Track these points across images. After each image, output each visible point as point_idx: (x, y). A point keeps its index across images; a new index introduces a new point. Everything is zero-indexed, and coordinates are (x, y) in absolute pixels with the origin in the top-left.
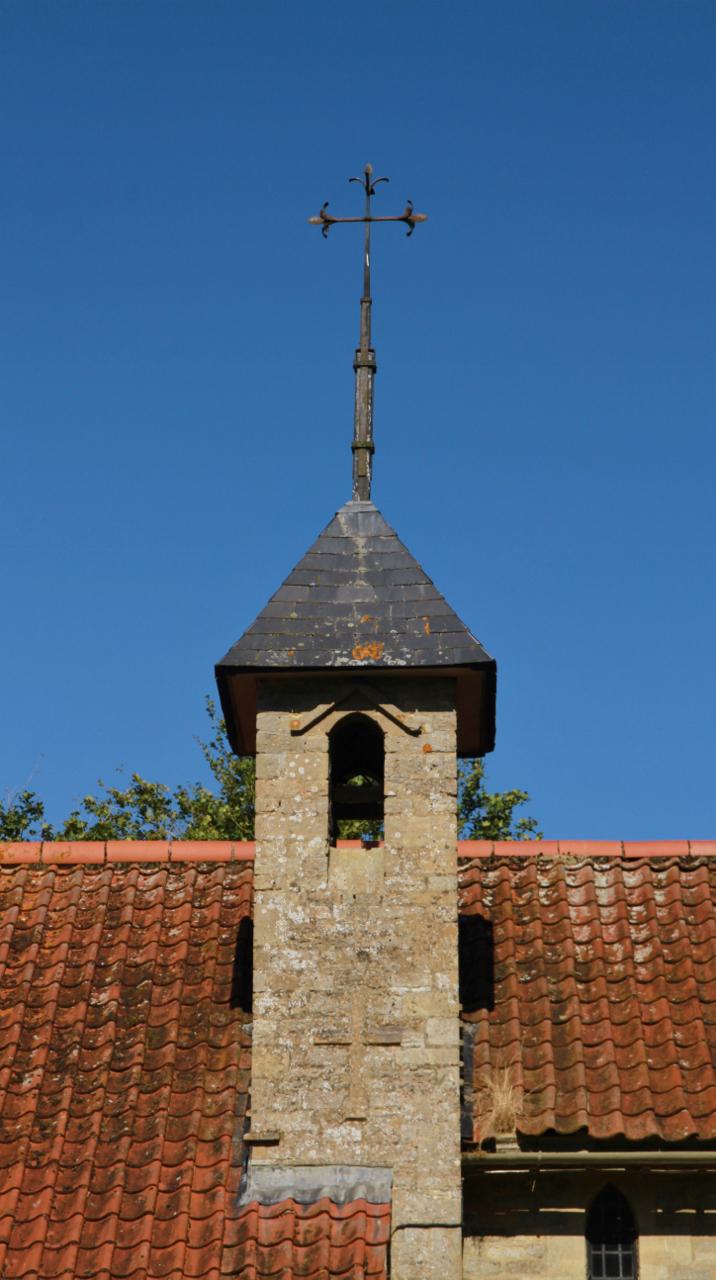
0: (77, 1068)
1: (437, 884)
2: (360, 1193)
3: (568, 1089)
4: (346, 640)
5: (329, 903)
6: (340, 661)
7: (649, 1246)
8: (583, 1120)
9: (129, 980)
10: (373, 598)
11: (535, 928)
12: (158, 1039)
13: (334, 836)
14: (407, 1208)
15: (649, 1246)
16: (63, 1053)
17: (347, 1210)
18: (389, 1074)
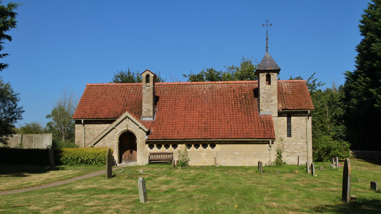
0: (242, 103)
1: (276, 88)
2: (269, 114)
3: (285, 105)
4: (267, 67)
5: (266, 90)
6: (267, 69)
7: (292, 118)
8: (287, 108)
9: (245, 95)
10: (269, 63)
11: (280, 89)
12: (249, 100)
13: (266, 85)
14: (273, 115)
15: (292, 118)
16: (241, 102)
17: (269, 116)
18: (272, 105)
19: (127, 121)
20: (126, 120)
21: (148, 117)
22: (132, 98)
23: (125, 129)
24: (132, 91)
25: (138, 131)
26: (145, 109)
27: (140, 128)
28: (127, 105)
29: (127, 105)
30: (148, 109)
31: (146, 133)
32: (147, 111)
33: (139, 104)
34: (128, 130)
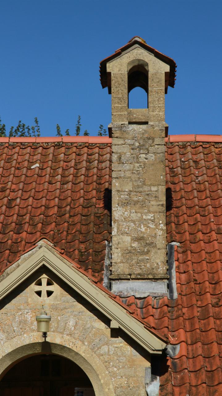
19: (44, 293)
20: (38, 288)
21: (141, 278)
22: (41, 195)
23: (36, 338)
24: (37, 165)
25: (105, 349)
26: (128, 239)
27: (117, 333)
28: (20, 225)
29: (20, 225)
30: (139, 239)
31: (148, 364)
32: (135, 245)
33: (77, 219)
34: (46, 345)
